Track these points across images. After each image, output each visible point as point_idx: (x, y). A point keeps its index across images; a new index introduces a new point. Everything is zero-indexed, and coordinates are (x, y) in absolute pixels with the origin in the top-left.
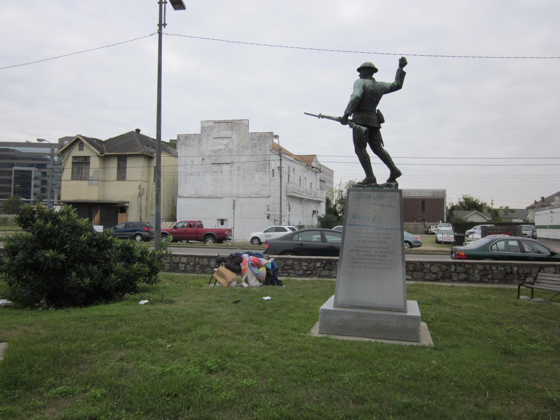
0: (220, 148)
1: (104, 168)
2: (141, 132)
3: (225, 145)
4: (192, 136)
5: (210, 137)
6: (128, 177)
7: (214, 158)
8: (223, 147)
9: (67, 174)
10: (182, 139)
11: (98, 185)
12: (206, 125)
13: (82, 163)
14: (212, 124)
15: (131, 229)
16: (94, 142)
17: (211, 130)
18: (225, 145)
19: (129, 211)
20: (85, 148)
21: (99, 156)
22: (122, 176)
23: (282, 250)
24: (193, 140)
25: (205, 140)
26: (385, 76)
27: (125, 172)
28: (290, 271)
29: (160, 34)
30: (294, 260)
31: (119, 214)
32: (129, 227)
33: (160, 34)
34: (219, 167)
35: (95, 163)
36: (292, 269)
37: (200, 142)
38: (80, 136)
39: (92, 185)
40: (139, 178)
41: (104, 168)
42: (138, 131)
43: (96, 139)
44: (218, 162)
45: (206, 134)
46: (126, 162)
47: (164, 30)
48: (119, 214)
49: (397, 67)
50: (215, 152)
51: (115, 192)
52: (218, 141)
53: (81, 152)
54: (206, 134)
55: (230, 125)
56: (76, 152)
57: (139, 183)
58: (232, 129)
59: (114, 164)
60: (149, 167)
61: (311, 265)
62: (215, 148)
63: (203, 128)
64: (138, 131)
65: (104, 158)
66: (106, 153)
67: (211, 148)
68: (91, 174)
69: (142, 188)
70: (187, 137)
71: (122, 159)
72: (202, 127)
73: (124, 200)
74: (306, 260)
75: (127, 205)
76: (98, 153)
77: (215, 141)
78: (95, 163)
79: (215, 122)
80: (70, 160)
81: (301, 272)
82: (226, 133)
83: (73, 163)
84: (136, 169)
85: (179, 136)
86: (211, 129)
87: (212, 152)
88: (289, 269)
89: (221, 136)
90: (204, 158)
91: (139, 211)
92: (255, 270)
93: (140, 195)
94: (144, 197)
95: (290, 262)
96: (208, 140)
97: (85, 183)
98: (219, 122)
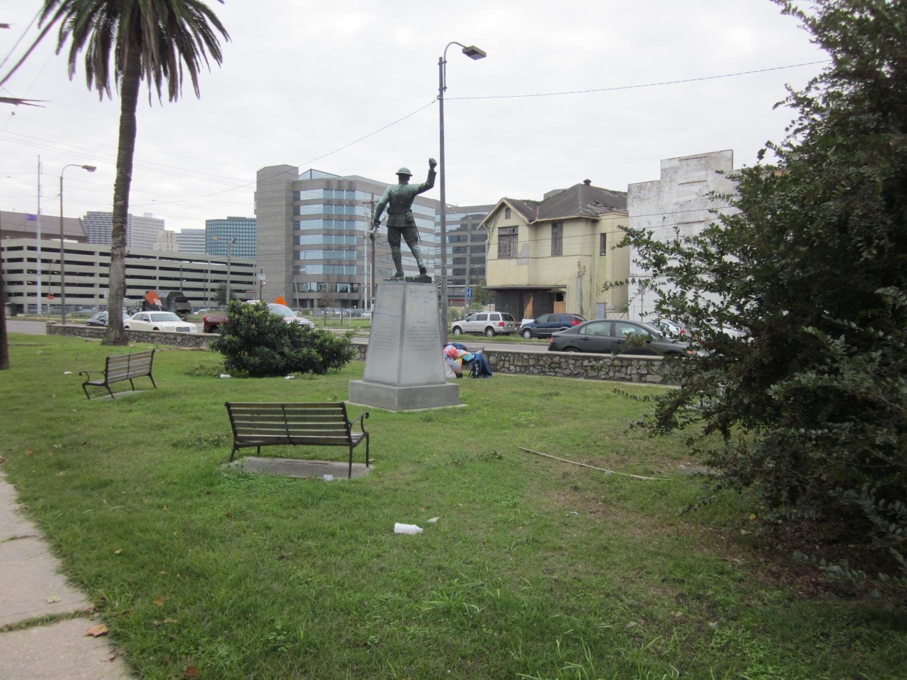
0: (688, 199)
1: (536, 240)
2: (591, 184)
3: (696, 193)
4: (649, 185)
5: (673, 183)
6: (565, 252)
7: (680, 214)
8: (693, 197)
9: (492, 251)
10: (635, 190)
11: (528, 264)
12: (667, 166)
13: (510, 234)
14: (676, 163)
15: (557, 322)
16: (523, 207)
17: (675, 172)
18: (696, 193)
19: (567, 298)
20: (512, 214)
21: (528, 225)
22: (557, 250)
23: (565, 345)
24: (649, 190)
25: (666, 189)
26: (418, 179)
27: (561, 245)
28: (557, 370)
29: (441, 99)
30: (561, 356)
31: (555, 303)
32: (554, 320)
33: (441, 99)
34: (688, 228)
35: (524, 234)
36: (559, 368)
37: (660, 192)
38: (506, 199)
39: (521, 264)
40: (578, 251)
41: (536, 240)
42: (587, 182)
43: (528, 202)
44: (686, 220)
45: (668, 179)
46: (561, 230)
47: (446, 94)
48: (555, 303)
49: (428, 167)
50: (681, 205)
51: (550, 272)
52: (686, 188)
53: (508, 220)
54: (668, 179)
55: (703, 161)
56: (502, 221)
57: (577, 259)
58: (706, 167)
59: (547, 233)
60: (594, 234)
61: (578, 363)
62: (682, 200)
63: (663, 171)
64: (587, 182)
65: (536, 226)
66: (538, 220)
67: (675, 200)
68: (520, 249)
69: (582, 266)
70: (641, 186)
71: (557, 225)
72: (662, 170)
73: (559, 284)
74: (573, 357)
75: (563, 290)
76: (526, 220)
77: (681, 188)
78: (524, 234)
79: (681, 160)
80: (496, 233)
81: (567, 372)
82: (698, 174)
83: (500, 236)
84: (575, 238)
85: (630, 186)
86: (675, 170)
87: (677, 206)
88: (556, 368)
89: (690, 180)
90: (666, 216)
91: (579, 297)
92: (452, 361)
93: (580, 276)
94: (586, 278)
95: (557, 359)
96: (670, 188)
97: (513, 262)
98: (687, 159)
